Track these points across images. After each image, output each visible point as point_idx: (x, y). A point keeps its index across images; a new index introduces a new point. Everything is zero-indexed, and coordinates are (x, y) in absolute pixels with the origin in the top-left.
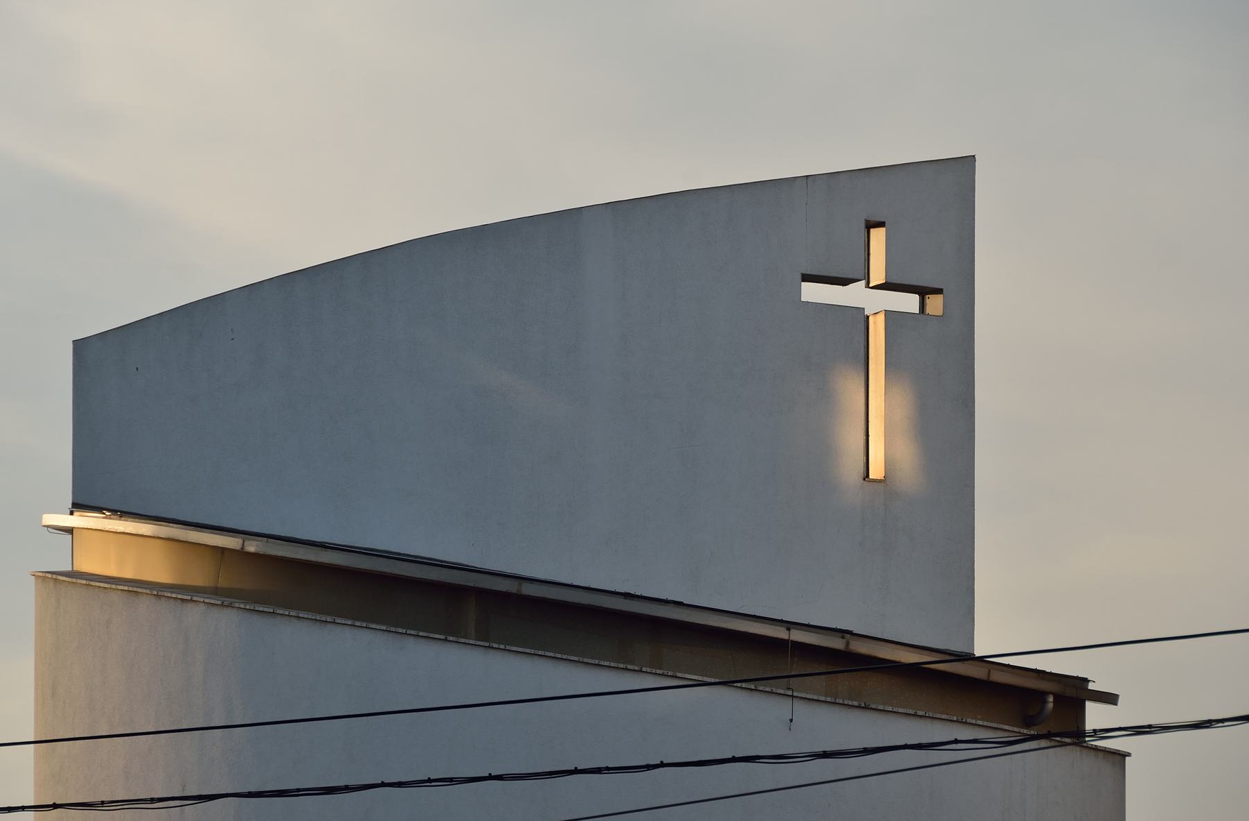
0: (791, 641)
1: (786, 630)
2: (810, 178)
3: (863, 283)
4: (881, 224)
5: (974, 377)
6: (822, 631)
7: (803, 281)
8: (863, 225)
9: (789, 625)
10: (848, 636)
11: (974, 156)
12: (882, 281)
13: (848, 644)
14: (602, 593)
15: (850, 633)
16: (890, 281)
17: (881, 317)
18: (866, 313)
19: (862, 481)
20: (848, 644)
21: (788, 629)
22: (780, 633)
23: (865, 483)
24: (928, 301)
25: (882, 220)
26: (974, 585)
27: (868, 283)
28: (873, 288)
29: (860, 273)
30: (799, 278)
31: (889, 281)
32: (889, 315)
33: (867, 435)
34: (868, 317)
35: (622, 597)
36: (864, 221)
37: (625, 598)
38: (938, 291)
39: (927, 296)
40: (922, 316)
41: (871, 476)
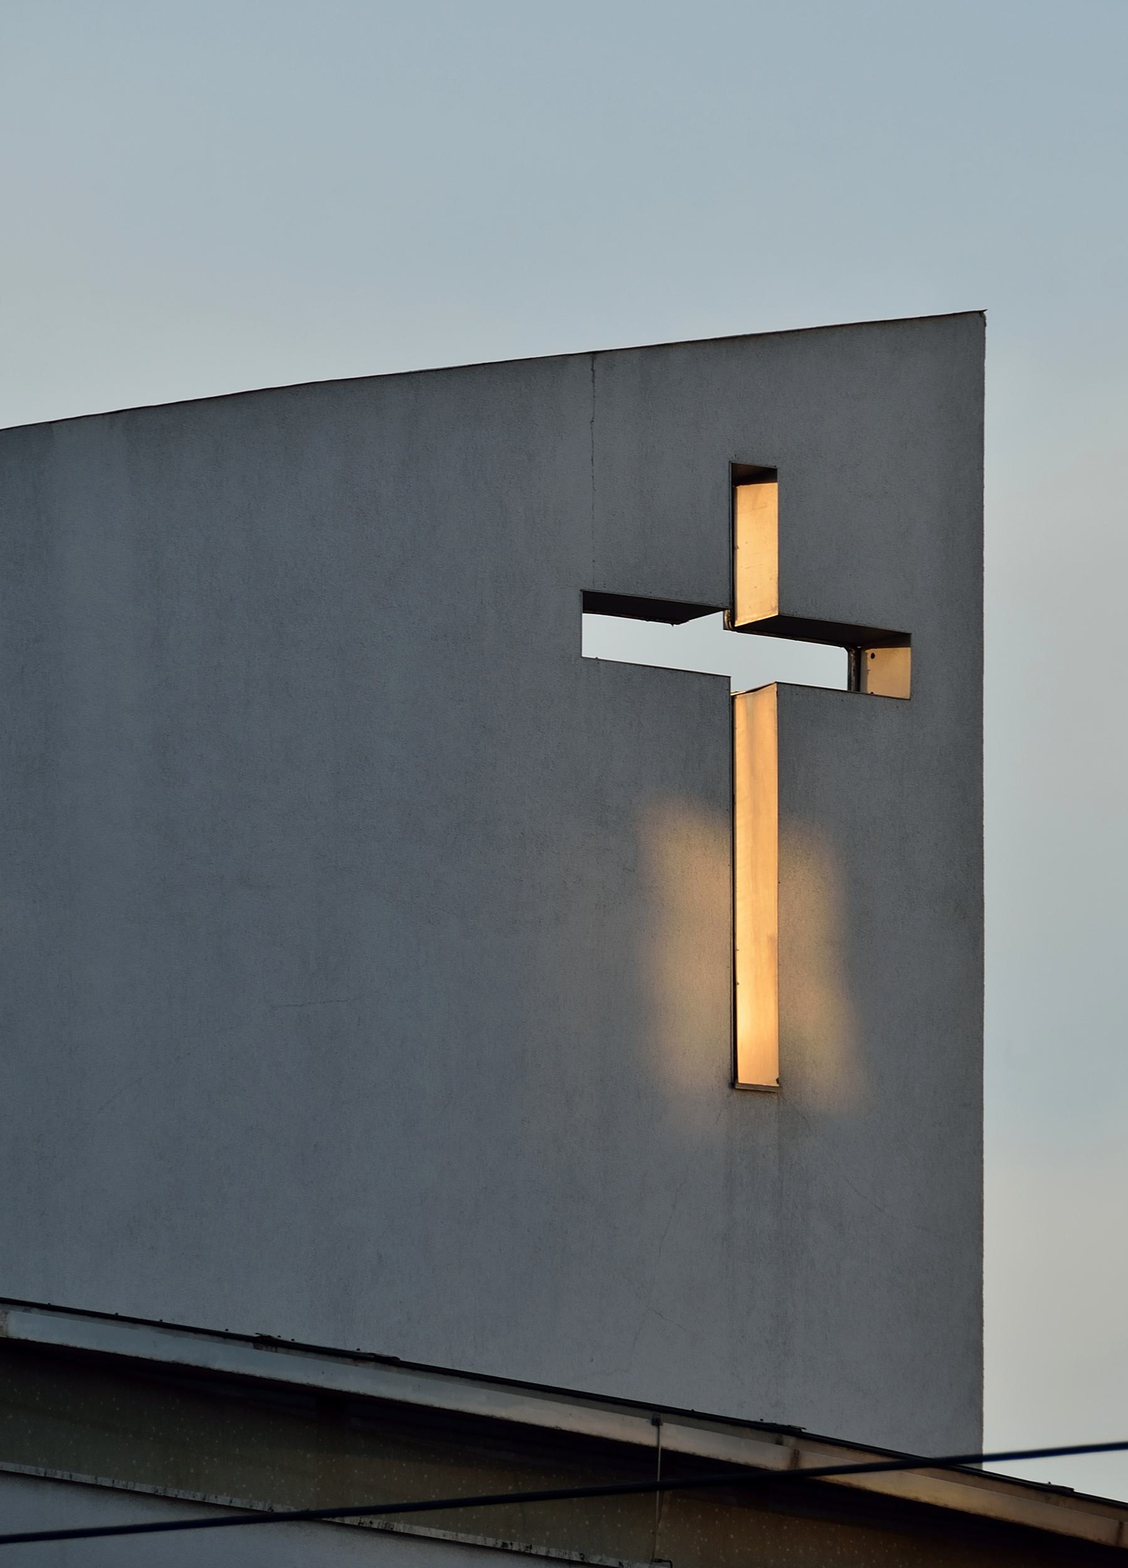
0: (665, 1451)
1: (649, 1425)
2: (599, 359)
3: (718, 617)
4: (763, 475)
5: (982, 846)
6: (730, 1428)
7: (584, 612)
8: (725, 476)
9: (658, 1414)
10: (790, 1440)
11: (981, 313)
12: (769, 611)
13: (796, 1456)
14: (202, 1336)
15: (794, 1432)
16: (790, 612)
17: (768, 705)
18: (734, 690)
19: (727, 1090)
20: (796, 1456)
21: (657, 1423)
22: (637, 1432)
23: (735, 1094)
24: (870, 664)
25: (770, 464)
26: (982, 1338)
27: (732, 617)
28: (744, 629)
29: (723, 600)
30: (577, 601)
31: (786, 613)
32: (785, 691)
33: (735, 984)
34: (733, 698)
35: (251, 1344)
36: (727, 464)
37: (255, 1347)
38: (898, 639)
39: (869, 652)
40: (855, 697)
41: (742, 1078)
